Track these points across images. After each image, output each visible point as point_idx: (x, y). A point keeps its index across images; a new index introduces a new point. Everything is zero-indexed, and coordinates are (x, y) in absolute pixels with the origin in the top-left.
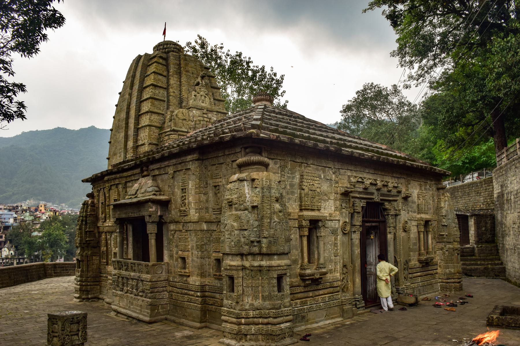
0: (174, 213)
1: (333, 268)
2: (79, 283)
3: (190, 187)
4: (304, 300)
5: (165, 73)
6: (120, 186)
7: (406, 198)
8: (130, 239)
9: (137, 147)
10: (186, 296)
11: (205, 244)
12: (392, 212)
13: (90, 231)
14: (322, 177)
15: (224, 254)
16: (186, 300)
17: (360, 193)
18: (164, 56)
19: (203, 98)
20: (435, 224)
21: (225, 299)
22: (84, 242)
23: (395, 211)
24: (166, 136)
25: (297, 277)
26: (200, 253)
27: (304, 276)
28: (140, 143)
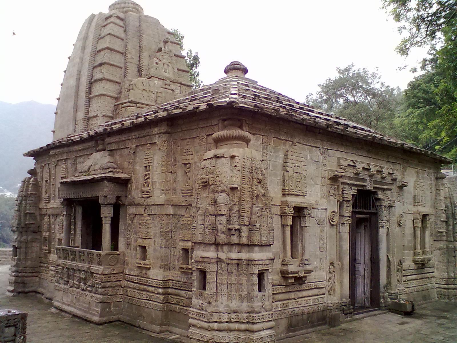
0: (135, 194)
1: (318, 265)
2: (14, 274)
3: (155, 165)
4: (285, 302)
5: (123, 35)
6: (69, 162)
7: (401, 187)
8: (79, 224)
9: (88, 119)
10: (145, 293)
11: (171, 231)
12: (386, 203)
13: (30, 213)
14: (309, 157)
15: (195, 243)
16: (144, 297)
17: (350, 178)
18: (122, 15)
19: (166, 66)
20: (432, 219)
21: (194, 297)
22: (23, 225)
23: (389, 202)
24: (122, 108)
26: (164, 241)
27: (285, 274)
28: (92, 114)
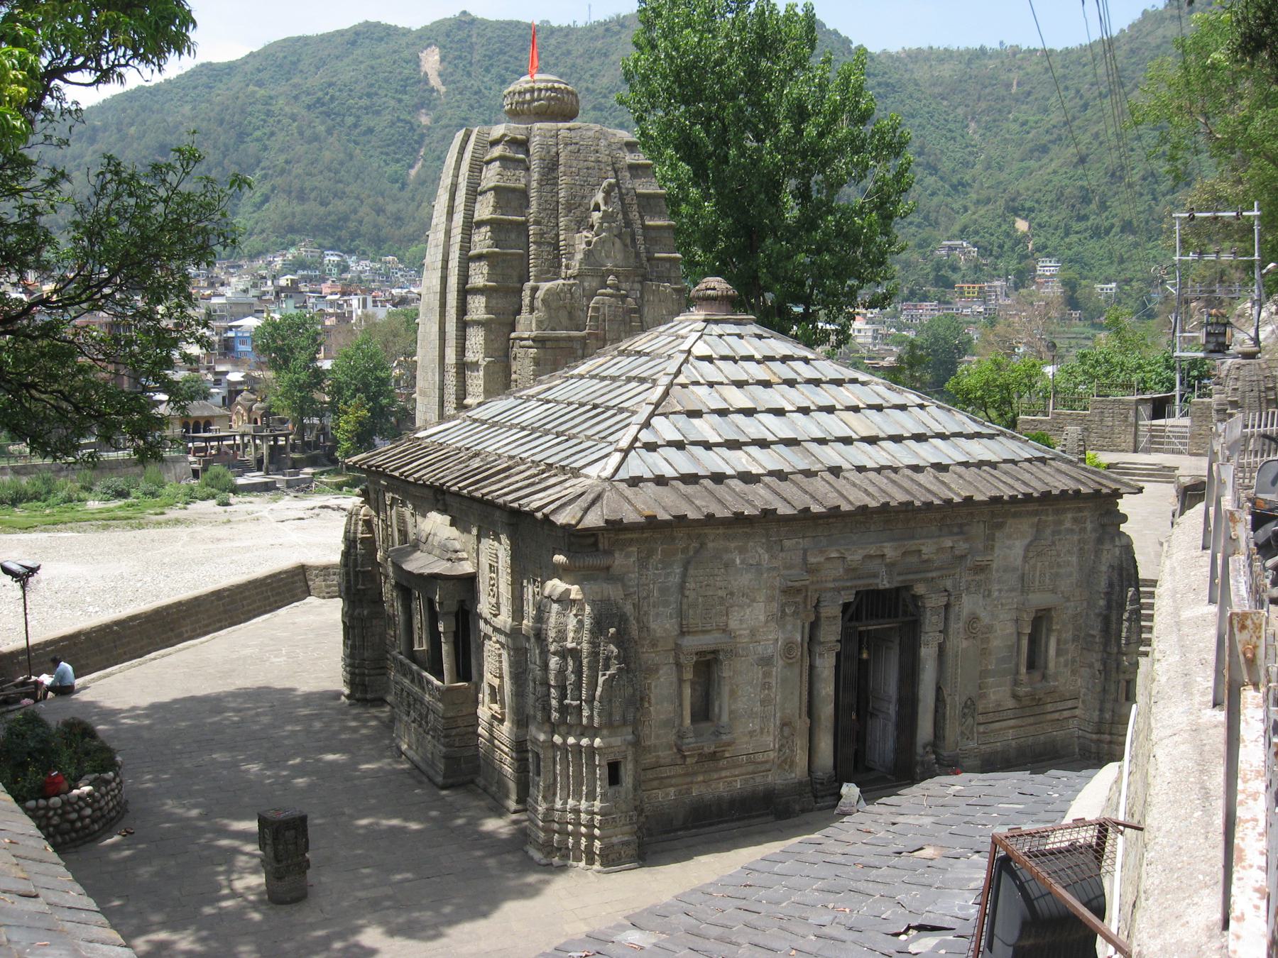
25: (671, 749)
